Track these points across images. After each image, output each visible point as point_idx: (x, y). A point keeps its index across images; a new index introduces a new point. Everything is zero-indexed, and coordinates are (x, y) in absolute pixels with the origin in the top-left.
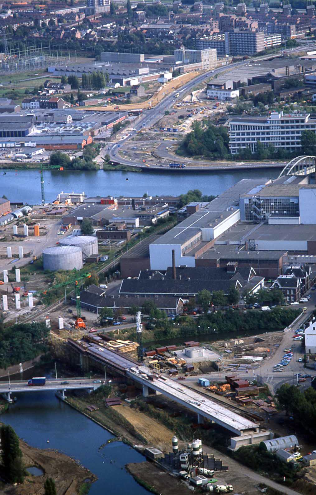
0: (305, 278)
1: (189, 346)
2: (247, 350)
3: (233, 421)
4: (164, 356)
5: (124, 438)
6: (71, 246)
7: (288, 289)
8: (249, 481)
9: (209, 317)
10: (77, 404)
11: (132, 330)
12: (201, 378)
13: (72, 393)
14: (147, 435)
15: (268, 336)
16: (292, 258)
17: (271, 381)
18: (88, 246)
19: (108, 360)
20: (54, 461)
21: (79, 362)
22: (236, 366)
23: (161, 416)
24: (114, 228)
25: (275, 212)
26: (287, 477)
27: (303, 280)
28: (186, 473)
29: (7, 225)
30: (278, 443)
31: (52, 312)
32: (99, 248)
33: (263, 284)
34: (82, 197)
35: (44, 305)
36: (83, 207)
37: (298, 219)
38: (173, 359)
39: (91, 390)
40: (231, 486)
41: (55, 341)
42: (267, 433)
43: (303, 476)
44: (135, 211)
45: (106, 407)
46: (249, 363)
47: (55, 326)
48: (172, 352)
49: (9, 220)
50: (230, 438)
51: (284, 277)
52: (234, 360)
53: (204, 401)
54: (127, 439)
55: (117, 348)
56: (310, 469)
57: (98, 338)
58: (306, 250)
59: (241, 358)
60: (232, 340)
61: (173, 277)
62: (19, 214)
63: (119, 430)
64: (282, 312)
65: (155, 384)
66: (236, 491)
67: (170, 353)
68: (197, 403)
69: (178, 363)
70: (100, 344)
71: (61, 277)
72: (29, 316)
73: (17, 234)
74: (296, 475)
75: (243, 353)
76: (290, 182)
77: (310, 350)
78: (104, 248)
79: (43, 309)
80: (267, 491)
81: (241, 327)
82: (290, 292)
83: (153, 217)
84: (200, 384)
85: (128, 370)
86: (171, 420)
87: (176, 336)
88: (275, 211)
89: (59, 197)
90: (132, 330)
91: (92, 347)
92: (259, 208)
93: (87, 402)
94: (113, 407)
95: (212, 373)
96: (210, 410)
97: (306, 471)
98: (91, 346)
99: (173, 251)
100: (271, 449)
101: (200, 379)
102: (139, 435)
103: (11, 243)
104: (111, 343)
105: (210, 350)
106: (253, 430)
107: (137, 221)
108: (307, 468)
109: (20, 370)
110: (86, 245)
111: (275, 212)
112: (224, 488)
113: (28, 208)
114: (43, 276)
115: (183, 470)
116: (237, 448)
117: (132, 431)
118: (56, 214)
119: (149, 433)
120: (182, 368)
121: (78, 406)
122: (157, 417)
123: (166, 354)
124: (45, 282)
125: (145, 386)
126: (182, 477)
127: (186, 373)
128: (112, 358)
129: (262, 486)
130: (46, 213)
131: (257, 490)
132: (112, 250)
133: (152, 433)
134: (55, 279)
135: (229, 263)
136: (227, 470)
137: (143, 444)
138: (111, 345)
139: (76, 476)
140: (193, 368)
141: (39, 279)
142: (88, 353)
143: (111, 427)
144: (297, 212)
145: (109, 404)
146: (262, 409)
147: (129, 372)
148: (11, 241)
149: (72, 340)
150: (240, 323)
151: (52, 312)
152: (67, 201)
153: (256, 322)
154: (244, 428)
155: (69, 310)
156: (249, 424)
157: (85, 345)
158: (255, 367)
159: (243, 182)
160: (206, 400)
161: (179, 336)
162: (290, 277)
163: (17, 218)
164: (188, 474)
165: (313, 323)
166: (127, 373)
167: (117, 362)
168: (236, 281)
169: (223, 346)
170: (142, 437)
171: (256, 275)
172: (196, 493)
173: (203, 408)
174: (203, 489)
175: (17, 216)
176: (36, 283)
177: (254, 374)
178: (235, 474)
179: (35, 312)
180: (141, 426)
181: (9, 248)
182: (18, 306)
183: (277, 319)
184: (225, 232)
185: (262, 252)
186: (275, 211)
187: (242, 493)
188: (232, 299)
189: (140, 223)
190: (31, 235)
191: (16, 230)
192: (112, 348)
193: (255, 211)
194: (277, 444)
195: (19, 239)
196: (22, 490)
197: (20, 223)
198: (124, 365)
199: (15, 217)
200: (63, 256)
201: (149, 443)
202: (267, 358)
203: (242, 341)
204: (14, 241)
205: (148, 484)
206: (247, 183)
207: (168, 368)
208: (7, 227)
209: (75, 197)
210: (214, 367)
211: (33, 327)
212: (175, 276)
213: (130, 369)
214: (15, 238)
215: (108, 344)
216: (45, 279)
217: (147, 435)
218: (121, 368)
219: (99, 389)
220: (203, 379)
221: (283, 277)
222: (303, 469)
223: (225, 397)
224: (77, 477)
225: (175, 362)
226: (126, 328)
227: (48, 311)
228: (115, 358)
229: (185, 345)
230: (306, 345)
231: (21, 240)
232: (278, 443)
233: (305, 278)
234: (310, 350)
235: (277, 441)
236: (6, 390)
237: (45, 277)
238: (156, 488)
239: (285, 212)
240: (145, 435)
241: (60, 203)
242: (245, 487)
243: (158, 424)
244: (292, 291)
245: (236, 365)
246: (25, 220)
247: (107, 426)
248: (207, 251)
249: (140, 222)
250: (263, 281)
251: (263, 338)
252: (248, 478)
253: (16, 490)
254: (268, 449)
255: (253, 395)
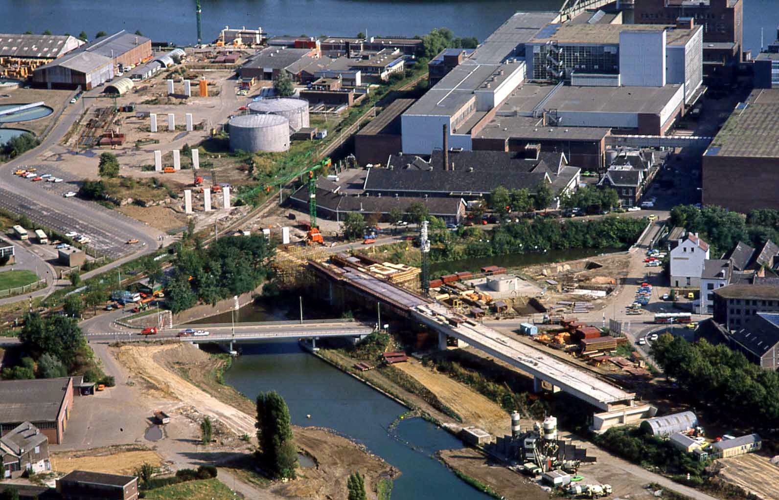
1: (490, 273)
2: (580, 281)
3: (594, 388)
4: (455, 287)
5: (423, 413)
6: (270, 113)
7: (625, 188)
8: (632, 479)
9: (509, 229)
10: (339, 360)
11: (395, 247)
12: (524, 322)
13: (326, 343)
14: (459, 408)
15: (607, 260)
16: (619, 140)
17: (629, 328)
18: (296, 115)
19: (380, 294)
20: (325, 445)
21: (327, 296)
22: (570, 305)
23: (475, 379)
24: (325, 86)
25: (580, 67)
26: (692, 474)
27: (644, 173)
28: (535, 466)
29: (152, 78)
30: (669, 423)
31: (263, 217)
32: (310, 117)
33: (578, 179)
34: (258, 36)
35: (248, 207)
36: (268, 52)
37: (617, 78)
38: (471, 292)
39: (357, 339)
40: (608, 486)
41: (283, 262)
42: (646, 408)
43: (717, 473)
44: (351, 60)
45: (384, 365)
46: (588, 301)
47: (277, 240)
48: (465, 282)
49: (154, 71)
50: (593, 416)
51: (618, 168)
52: (563, 296)
53: (542, 358)
54: (429, 414)
55: (388, 275)
56: (726, 462)
57: (354, 260)
58: (636, 126)
59: (574, 293)
60: (553, 265)
61: (444, 168)
62: (168, 61)
63: (412, 399)
64: (619, 222)
65: (460, 332)
66: (616, 495)
67: (463, 283)
68: (531, 362)
69: (479, 299)
70: (359, 268)
71: (263, 163)
72: (228, 224)
73: (173, 92)
74: (705, 470)
75: (576, 285)
76: (598, 20)
77: (677, 282)
78: (319, 118)
79: (248, 213)
80: (662, 494)
81: (557, 245)
83: (382, 69)
84: (522, 332)
85: (413, 309)
86: (491, 386)
87: (460, 257)
89: (223, 35)
90: (395, 247)
91: (349, 274)
92: (557, 60)
93: (353, 357)
94: (395, 364)
95: (535, 314)
96: (553, 371)
97: (720, 466)
98: (348, 272)
100: (659, 432)
101: (522, 324)
102: (448, 409)
103: (167, 106)
104: (376, 267)
105: (523, 279)
106: (626, 403)
107: (358, 75)
108: (720, 460)
109: (234, 306)
110: (293, 113)
111: (580, 67)
112: (598, 489)
113: (180, 52)
114: (233, 159)
115: (529, 461)
116: (603, 431)
117: (435, 403)
118: (225, 62)
119: (461, 405)
120: (488, 307)
121: (341, 363)
122: (469, 381)
123: (457, 284)
124: (238, 169)
125: (443, 333)
126: (528, 473)
127: (496, 314)
128: (382, 290)
129: (654, 487)
130: (209, 60)
131: (648, 493)
132: (329, 121)
133: (466, 406)
134: (254, 165)
135: (528, 147)
136: (594, 463)
137: (455, 422)
138: (376, 270)
139: (366, 469)
140: (506, 307)
141: (228, 164)
142: (344, 283)
143: (401, 396)
144: (615, 67)
145: (390, 360)
146: (627, 371)
147: (416, 312)
148: (166, 104)
149: (315, 262)
150: (556, 238)
151: (263, 217)
152: (237, 42)
153: (580, 237)
154: (613, 400)
155: (290, 214)
156: (620, 394)
157: (337, 270)
158: (599, 307)
159: (518, 18)
160: (545, 357)
161: (466, 257)
162: (628, 168)
163: (165, 67)
164: (538, 467)
165: (683, 241)
166: (413, 313)
167: (394, 297)
168: (545, 173)
169: (542, 274)
170: (453, 412)
171: (567, 165)
172: (556, 496)
173: (542, 368)
174: (565, 492)
175: (166, 64)
176: (225, 171)
177: (604, 318)
178: (607, 468)
179: (237, 216)
180: (447, 394)
181: (172, 115)
182: (208, 208)
183: (611, 233)
185: (571, 128)
187: (626, 497)
188: (541, 202)
189: (363, 79)
190: (195, 95)
191: (172, 87)
192: (381, 276)
193: (550, 63)
194: (667, 424)
195: (179, 100)
196: (298, 489)
197: (173, 75)
198: (405, 302)
199: (163, 65)
200: (262, 130)
201: (464, 420)
202: (613, 293)
203: (567, 267)
204: (171, 104)
205: (480, 483)
206: (524, 19)
207: (467, 307)
208: (153, 81)
209: (248, 36)
210: (535, 306)
211: (254, 241)
212: (447, 165)
213: (417, 308)
214: (173, 100)
215: (373, 268)
216: (238, 165)
217: (459, 408)
218: (402, 306)
219: (370, 338)
220: (526, 323)
221: (617, 169)
222: (715, 461)
223: (566, 352)
224: (369, 470)
225: (476, 298)
226: (384, 244)
227: (258, 216)
228: (388, 290)
229: (483, 271)
230: (672, 274)
231: (181, 103)
232: (669, 423)
234: (677, 282)
235: (666, 420)
236: (228, 337)
237: (237, 162)
238: (493, 489)
239: (596, 67)
240: (455, 408)
241: (225, 44)
242: (629, 488)
243: (473, 392)
245: (570, 303)
246: (180, 71)
247: (392, 394)
248: (487, 127)
249: (362, 77)
250: (578, 173)
251: (600, 261)
252: (629, 474)
253: (288, 488)
254: (655, 431)
255: (608, 350)
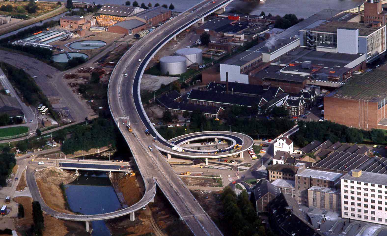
0: (310, 99)
7: (293, 107)
37: (336, 49)
82: (294, 109)
88: (323, 41)
92: (312, 39)
99: (227, 73)
184: (282, 56)
186: (323, 41)
233: (310, 99)
244: (296, 109)
